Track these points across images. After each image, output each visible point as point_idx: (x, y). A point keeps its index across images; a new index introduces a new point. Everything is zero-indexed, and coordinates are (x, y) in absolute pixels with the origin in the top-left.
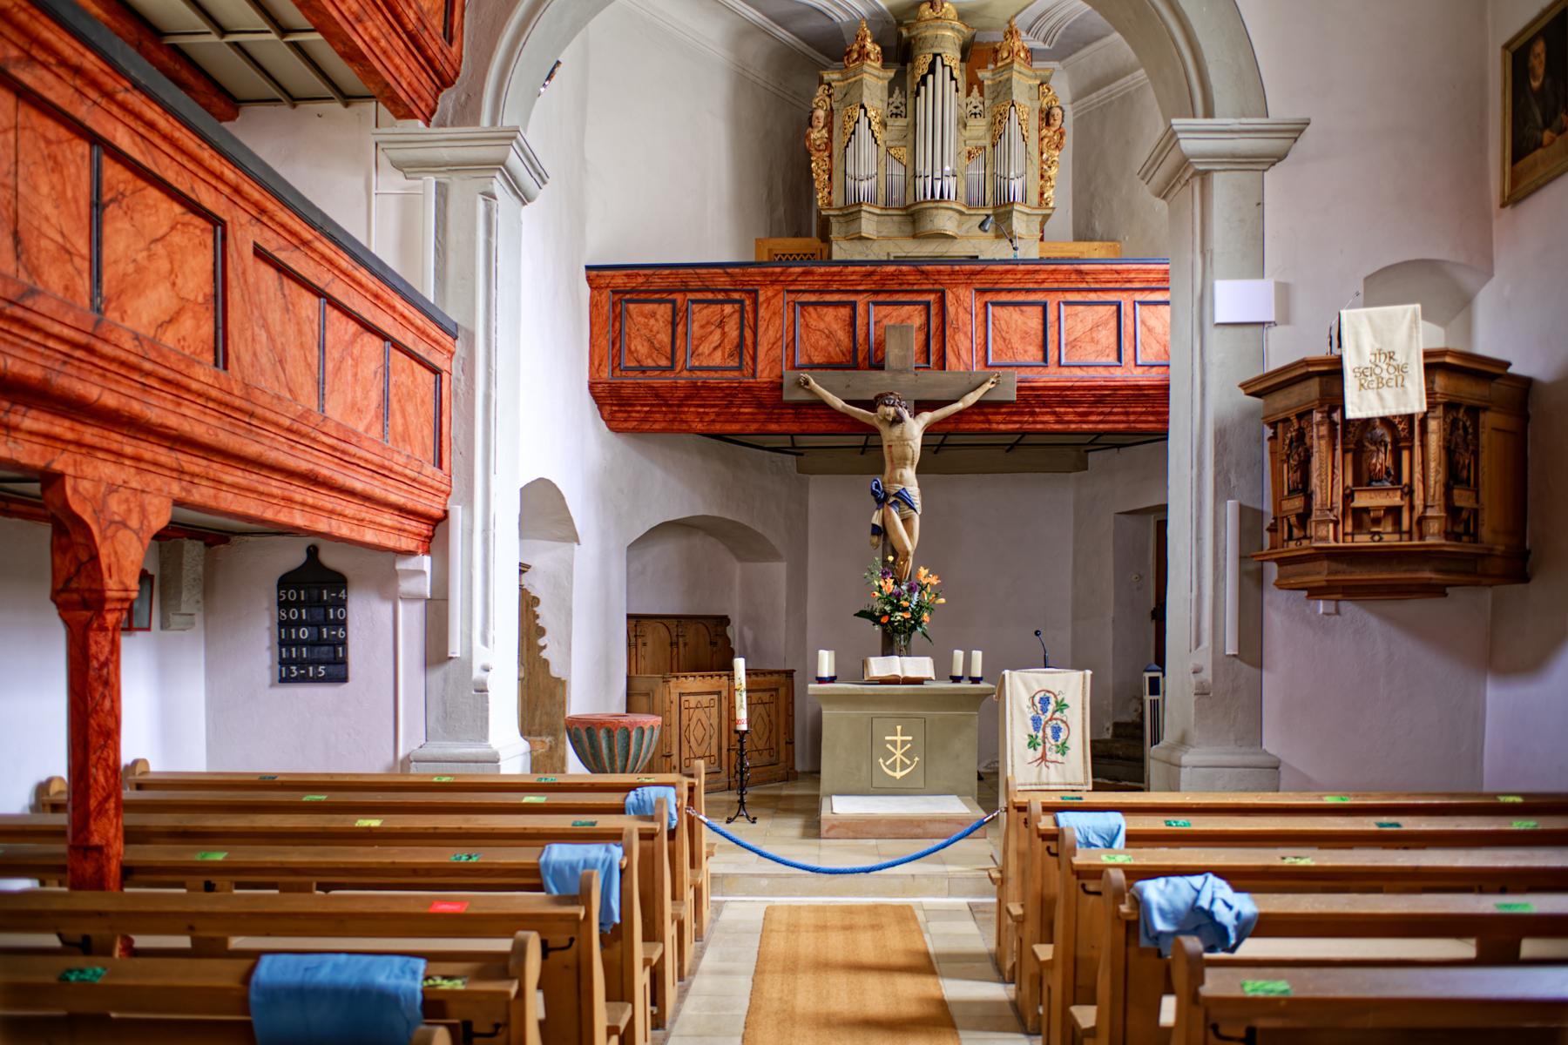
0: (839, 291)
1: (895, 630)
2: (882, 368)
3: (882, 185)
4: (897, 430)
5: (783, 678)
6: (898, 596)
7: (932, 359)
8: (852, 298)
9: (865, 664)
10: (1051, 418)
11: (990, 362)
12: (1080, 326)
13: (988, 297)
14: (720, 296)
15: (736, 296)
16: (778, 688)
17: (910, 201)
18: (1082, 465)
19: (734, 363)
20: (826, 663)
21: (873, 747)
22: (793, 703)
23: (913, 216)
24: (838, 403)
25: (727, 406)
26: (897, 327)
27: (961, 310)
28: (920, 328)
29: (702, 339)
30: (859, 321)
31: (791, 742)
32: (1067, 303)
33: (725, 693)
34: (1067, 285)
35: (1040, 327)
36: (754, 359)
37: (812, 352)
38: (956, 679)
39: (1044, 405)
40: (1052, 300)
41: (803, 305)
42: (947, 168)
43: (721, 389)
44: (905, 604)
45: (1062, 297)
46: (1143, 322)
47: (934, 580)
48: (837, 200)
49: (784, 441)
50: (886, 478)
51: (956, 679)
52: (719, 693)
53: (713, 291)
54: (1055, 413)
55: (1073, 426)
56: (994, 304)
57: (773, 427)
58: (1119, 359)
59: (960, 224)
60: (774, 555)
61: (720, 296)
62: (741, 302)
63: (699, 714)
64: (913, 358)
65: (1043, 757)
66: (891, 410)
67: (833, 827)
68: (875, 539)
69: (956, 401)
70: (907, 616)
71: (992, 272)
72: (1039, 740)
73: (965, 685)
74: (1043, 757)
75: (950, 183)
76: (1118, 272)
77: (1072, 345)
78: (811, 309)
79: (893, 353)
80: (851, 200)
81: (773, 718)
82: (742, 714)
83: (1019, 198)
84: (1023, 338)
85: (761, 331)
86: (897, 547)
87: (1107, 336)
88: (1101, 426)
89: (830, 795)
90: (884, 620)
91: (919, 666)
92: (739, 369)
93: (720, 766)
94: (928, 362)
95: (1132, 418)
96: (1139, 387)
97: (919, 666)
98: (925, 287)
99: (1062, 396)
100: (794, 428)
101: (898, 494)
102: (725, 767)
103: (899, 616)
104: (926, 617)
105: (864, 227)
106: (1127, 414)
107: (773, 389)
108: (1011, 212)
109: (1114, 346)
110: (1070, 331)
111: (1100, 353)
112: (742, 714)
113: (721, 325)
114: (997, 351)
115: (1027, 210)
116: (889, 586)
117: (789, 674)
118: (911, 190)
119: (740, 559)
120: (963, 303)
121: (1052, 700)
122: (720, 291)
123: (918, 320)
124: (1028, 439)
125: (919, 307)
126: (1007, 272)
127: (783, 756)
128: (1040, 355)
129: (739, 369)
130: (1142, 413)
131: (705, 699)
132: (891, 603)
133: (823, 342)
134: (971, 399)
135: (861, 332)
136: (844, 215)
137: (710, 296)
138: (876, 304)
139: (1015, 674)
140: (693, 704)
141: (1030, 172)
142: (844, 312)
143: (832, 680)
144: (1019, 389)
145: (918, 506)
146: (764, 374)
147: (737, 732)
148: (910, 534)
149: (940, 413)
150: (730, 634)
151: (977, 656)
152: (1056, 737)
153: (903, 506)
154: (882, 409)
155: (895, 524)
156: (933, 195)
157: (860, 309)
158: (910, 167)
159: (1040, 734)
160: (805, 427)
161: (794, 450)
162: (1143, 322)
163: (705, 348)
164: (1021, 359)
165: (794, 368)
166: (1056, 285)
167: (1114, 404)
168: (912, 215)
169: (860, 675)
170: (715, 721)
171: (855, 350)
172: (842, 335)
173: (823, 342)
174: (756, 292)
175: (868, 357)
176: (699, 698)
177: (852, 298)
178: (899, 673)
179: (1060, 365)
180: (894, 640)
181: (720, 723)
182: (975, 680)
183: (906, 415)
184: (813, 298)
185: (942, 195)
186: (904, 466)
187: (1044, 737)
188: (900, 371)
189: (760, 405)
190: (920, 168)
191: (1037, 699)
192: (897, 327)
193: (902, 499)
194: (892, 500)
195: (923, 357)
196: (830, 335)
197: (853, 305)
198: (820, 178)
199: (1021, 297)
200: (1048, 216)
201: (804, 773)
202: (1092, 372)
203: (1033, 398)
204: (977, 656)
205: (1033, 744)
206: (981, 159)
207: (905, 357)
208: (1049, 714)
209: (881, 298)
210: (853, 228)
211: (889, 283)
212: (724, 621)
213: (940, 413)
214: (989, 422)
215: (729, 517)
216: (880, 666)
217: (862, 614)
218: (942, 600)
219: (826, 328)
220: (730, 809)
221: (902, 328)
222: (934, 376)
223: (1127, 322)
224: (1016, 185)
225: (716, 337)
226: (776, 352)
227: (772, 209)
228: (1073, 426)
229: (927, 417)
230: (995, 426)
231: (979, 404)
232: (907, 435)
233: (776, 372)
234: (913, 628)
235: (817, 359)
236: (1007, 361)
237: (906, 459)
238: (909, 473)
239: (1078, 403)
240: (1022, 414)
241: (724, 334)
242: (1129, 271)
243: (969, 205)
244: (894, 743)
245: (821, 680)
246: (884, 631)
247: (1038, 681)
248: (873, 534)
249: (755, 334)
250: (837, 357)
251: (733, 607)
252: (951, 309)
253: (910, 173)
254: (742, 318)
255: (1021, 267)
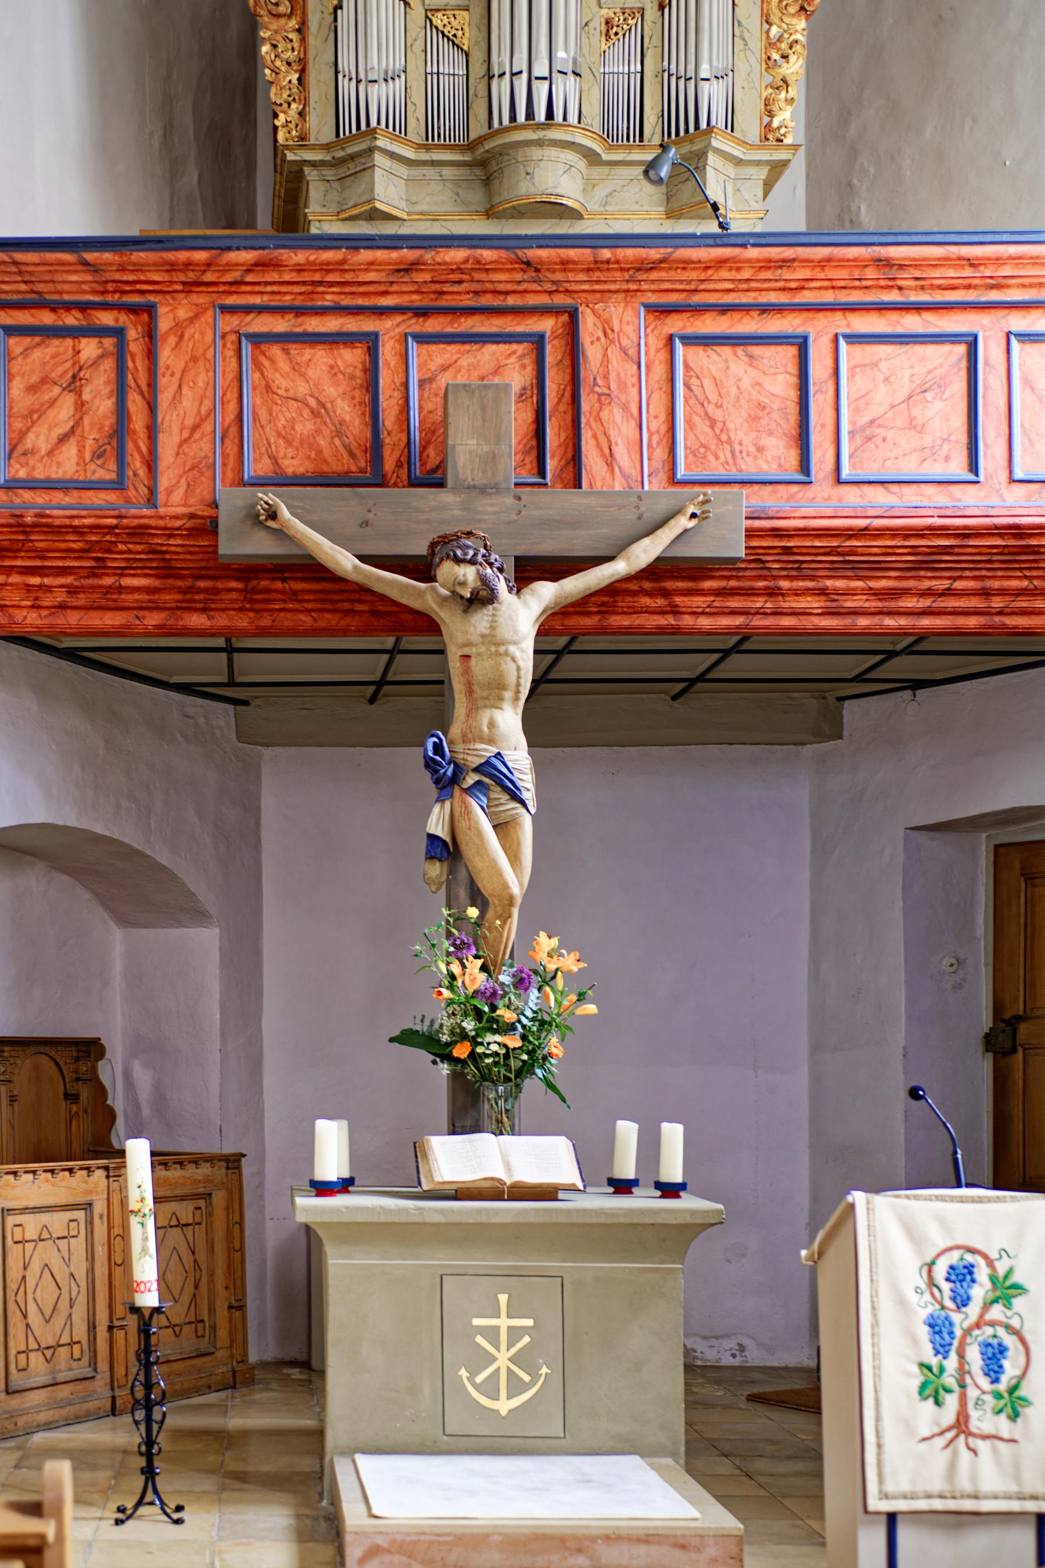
0: (338, 310)
1: (486, 1076)
2: (441, 484)
3: (417, 97)
4: (480, 621)
5: (219, 1172)
6: (491, 998)
7: (551, 464)
8: (368, 325)
9: (418, 1152)
10: (815, 603)
11: (681, 473)
12: (882, 388)
13: (676, 324)
14: (71, 319)
15: (106, 318)
16: (210, 1191)
17: (478, 129)
18: (830, 728)
19: (106, 472)
20: (332, 1151)
21: (443, 1340)
22: (241, 1224)
23: (485, 161)
24: (344, 561)
25: (93, 573)
26: (474, 392)
27: (613, 353)
28: (521, 396)
29: (34, 416)
30: (386, 379)
31: (238, 1307)
32: (854, 339)
33: (100, 1207)
34: (855, 297)
35: (793, 394)
36: (151, 464)
37: (281, 449)
38: (622, 1187)
39: (798, 571)
40: (820, 331)
41: (259, 340)
42: (561, 54)
43: (76, 530)
44: (509, 1016)
45: (842, 323)
46: (1027, 382)
47: (570, 962)
48: (320, 128)
49: (210, 668)
50: (456, 730)
51: (622, 1187)
52: (88, 1207)
53: (54, 308)
54: (823, 592)
55: (863, 622)
56: (689, 340)
57: (196, 620)
58: (973, 466)
59: (589, 185)
60: (198, 916)
61: (71, 319)
62: (118, 333)
63: (46, 1253)
64: (511, 462)
65: (961, 1424)
66: (469, 573)
67: (374, 1552)
68: (435, 870)
69: (610, 559)
70: (514, 1042)
71: (686, 264)
72: (949, 1380)
73: (643, 1201)
74: (961, 1424)
75: (566, 89)
76: (973, 263)
77: (866, 434)
78: (276, 351)
79: (465, 449)
80: (349, 127)
81: (202, 1255)
82: (146, 1269)
83: (719, 119)
84: (753, 419)
85: (164, 399)
86: (485, 885)
87: (946, 414)
88: (926, 622)
89: (350, 1452)
90: (461, 1051)
91: (542, 1157)
92: (118, 485)
93: (93, 1364)
94: (542, 472)
95: (997, 603)
96: (1017, 531)
97: (542, 1157)
98: (532, 300)
99: (845, 551)
100: (243, 622)
101: (485, 768)
102: (103, 1366)
103: (493, 1043)
104: (554, 1044)
105: (379, 190)
106: (986, 593)
107: (195, 532)
108: (701, 156)
109: (961, 437)
110: (861, 401)
111: (928, 453)
112: (146, 1269)
113: (75, 383)
114: (710, 443)
115: (738, 152)
116: (474, 977)
117: (233, 1162)
118: (479, 108)
119: (124, 921)
120: (619, 338)
121: (982, 1273)
122: (68, 307)
123: (517, 377)
124: (738, 665)
125: (520, 348)
126: (720, 263)
127: (223, 1334)
128: (792, 457)
129: (118, 485)
130: (1020, 593)
131: (58, 1222)
132: (478, 1014)
133: (305, 427)
134: (645, 553)
135: (389, 417)
136: (337, 163)
137: (47, 318)
138: (423, 339)
139: (883, 1202)
140: (31, 1233)
141: (742, 68)
142: (351, 357)
143: (345, 1186)
144: (750, 533)
145: (529, 796)
146: (176, 500)
147: (135, 1310)
148: (514, 859)
149: (575, 585)
150: (105, 1078)
151: (673, 1134)
152: (993, 1371)
153: (497, 793)
154: (447, 570)
155: (480, 834)
156: (530, 115)
157: (387, 352)
158: (478, 57)
159: (952, 1363)
160: (266, 621)
161: (229, 692)
162: (1027, 382)
163: (40, 439)
164: (750, 468)
165: (242, 483)
166: (829, 297)
167: (957, 571)
168: (482, 164)
169: (405, 1171)
170: (80, 1268)
171: (376, 447)
172: (347, 411)
173: (305, 427)
174: (150, 310)
175: (406, 461)
176: (45, 1218)
177: (368, 325)
178: (500, 1173)
179: (839, 481)
180: (476, 1097)
181: (91, 1271)
182: (670, 1191)
183: (502, 587)
184: (280, 325)
185: (550, 114)
186: (497, 702)
187: (963, 1370)
188: (483, 490)
189: (167, 571)
190: (500, 60)
191: (941, 1271)
192: (474, 392)
193: (495, 776)
194: (471, 779)
195: (531, 460)
196: (320, 410)
197: (371, 343)
198: (279, 82)
199: (749, 325)
200: (784, 164)
201: (264, 1365)
202: (910, 496)
203: (783, 553)
204: (673, 1134)
205: (932, 1391)
206: (634, 39)
207: (492, 458)
208: (973, 1310)
209: (433, 325)
210: (356, 192)
211: (446, 295)
212: (91, 1049)
213: (575, 585)
214: (675, 611)
215: (99, 829)
216: (457, 1157)
217: (407, 1038)
218: (591, 1009)
219: (309, 394)
220: (120, 1473)
221: (487, 392)
222: (555, 501)
223: (991, 382)
224: (713, 94)
225: (64, 412)
226: (201, 447)
227: (174, 173)
228: (863, 622)
229: (546, 593)
230: (687, 621)
231: (658, 571)
232: (504, 632)
233: (202, 492)
234: (525, 1070)
235: (293, 465)
236: (719, 471)
237: (502, 687)
238: (509, 720)
239: (877, 568)
240: (750, 593)
241: (81, 406)
242: (998, 261)
243: (608, 136)
244: (492, 1334)
245: (323, 1189)
246: (457, 1078)
247: (942, 1221)
248: (430, 857)
249: (152, 407)
250: (339, 463)
251: (112, 1024)
252: (592, 352)
253: (478, 70)
254: (121, 370)
255: (753, 253)
